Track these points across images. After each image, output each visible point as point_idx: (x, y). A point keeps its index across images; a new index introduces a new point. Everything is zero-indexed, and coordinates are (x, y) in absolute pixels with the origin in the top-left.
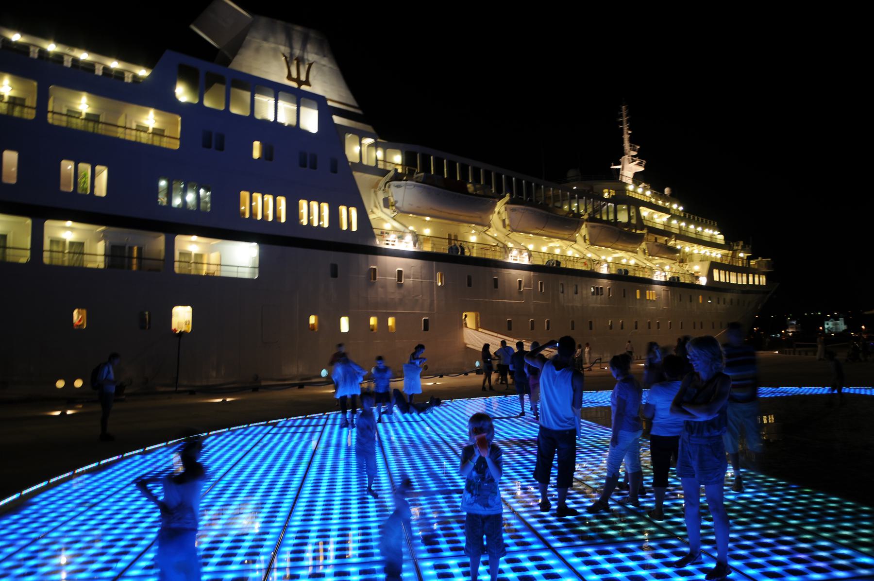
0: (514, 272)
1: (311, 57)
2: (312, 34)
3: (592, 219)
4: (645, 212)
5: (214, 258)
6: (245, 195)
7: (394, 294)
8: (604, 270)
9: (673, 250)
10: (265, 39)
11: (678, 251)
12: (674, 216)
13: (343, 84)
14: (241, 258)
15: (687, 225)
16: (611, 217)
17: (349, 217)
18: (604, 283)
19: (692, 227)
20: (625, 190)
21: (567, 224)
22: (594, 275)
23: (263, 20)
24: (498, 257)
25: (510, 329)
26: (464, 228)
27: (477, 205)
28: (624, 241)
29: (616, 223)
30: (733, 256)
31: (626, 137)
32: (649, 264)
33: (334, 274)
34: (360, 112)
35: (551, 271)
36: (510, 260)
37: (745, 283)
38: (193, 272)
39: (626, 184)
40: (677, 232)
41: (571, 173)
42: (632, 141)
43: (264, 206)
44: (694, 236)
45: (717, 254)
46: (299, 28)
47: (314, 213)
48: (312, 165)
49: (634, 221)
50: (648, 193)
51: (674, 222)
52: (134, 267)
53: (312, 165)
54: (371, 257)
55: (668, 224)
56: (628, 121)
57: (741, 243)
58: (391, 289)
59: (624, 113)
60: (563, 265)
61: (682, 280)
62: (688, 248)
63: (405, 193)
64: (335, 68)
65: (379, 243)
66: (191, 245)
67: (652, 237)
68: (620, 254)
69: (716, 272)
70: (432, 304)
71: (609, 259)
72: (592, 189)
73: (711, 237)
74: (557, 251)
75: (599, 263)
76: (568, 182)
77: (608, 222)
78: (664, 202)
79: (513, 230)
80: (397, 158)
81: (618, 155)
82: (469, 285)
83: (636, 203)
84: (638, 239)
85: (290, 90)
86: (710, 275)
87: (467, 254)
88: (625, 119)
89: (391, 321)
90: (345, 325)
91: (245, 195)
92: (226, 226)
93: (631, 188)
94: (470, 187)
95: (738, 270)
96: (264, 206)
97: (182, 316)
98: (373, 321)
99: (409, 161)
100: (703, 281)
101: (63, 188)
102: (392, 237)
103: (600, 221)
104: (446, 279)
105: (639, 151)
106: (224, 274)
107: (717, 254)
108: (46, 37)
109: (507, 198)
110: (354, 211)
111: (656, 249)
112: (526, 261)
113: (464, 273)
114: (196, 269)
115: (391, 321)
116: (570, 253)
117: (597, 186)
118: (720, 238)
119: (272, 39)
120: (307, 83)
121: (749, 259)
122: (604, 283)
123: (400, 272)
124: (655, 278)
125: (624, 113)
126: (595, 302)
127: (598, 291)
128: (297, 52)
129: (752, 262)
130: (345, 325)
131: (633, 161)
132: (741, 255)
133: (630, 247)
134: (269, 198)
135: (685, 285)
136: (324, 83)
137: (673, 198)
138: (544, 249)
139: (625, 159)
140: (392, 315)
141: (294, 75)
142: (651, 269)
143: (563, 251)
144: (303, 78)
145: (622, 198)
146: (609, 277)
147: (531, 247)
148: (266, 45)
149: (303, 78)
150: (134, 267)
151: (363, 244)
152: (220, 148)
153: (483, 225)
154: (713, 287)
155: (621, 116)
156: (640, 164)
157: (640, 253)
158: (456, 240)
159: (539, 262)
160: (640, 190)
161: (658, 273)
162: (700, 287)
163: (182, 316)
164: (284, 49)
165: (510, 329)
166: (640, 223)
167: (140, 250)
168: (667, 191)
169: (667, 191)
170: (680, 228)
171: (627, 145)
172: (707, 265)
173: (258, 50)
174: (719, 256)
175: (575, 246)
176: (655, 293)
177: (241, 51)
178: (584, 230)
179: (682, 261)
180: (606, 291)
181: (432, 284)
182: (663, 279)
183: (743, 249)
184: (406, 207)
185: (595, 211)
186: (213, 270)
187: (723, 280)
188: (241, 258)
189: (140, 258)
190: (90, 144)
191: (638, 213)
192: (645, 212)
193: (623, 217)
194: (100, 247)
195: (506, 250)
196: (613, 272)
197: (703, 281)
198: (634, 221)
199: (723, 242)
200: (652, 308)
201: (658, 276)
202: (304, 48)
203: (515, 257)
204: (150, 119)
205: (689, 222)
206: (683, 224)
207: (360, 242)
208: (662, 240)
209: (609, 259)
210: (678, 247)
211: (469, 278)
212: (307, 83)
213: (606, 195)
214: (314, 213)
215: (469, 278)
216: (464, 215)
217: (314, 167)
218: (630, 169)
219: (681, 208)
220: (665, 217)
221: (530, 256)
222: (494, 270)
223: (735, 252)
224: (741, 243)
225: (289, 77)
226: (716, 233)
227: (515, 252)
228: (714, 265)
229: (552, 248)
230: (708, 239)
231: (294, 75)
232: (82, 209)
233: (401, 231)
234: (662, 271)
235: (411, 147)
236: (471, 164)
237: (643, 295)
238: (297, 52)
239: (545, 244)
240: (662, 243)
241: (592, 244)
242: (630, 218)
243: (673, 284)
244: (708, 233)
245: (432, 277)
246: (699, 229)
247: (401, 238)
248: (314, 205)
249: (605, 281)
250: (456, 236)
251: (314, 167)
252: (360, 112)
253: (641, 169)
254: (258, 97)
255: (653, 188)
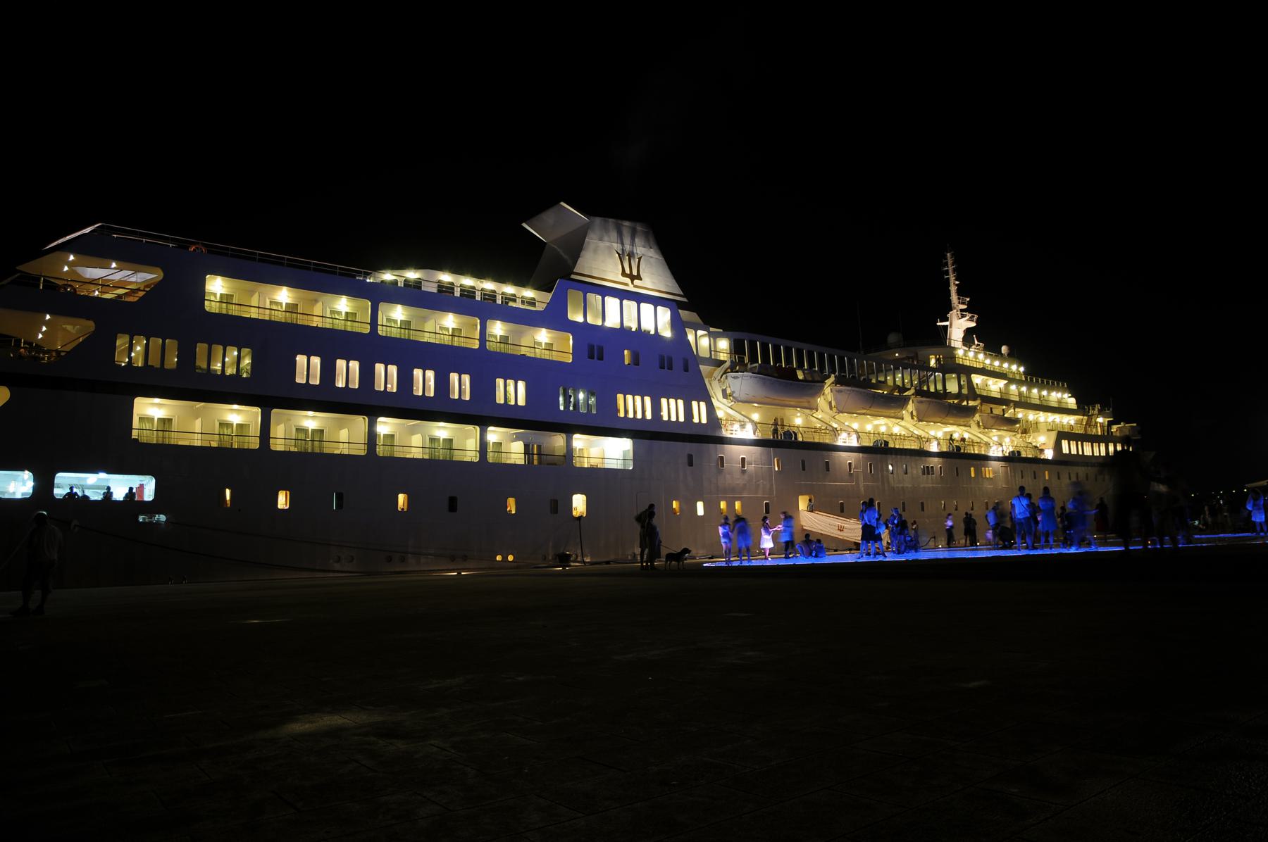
0: (844, 454)
1: (640, 250)
2: (639, 228)
3: (920, 393)
4: (977, 379)
5: (594, 452)
6: (620, 397)
7: (739, 480)
8: (934, 448)
9: (1013, 421)
10: (601, 240)
11: (1016, 421)
12: (1011, 381)
13: (668, 273)
14: (612, 452)
15: (1029, 390)
16: (940, 387)
17: (700, 413)
18: (935, 462)
19: (1035, 391)
20: (953, 357)
21: (892, 402)
22: (923, 453)
23: (598, 220)
24: (827, 440)
25: (842, 511)
26: (789, 412)
27: (808, 389)
28: (955, 416)
29: (946, 395)
30: (1088, 424)
31: (953, 289)
32: (985, 439)
33: (691, 464)
34: (685, 300)
35: (879, 451)
36: (840, 443)
37: (1103, 454)
38: (317, 450)
39: (954, 349)
40: (1017, 399)
41: (892, 338)
42: (960, 293)
43: (634, 406)
44: (1038, 402)
45: (1069, 421)
46: (627, 223)
47: (673, 410)
48: (671, 368)
49: (965, 391)
50: (981, 356)
51: (1013, 387)
52: (536, 462)
53: (671, 368)
54: (719, 446)
55: (1005, 392)
56: (954, 270)
57: (1098, 407)
58: (737, 475)
59: (950, 262)
60: (891, 445)
61: (1023, 455)
62: (1032, 416)
63: (742, 383)
64: (661, 258)
65: (726, 433)
66: (579, 441)
67: (986, 407)
68: (950, 428)
69: (1065, 443)
70: (771, 489)
71: (938, 435)
72: (916, 357)
73: (1059, 402)
74: (883, 429)
75: (928, 440)
76: (890, 348)
77: (936, 395)
78: (1002, 363)
79: (840, 412)
80: (724, 344)
81: (944, 310)
82: (804, 469)
83: (968, 371)
84: (970, 412)
85: (629, 289)
86: (1058, 447)
87: (800, 439)
88: (951, 268)
89: (738, 505)
90: (700, 509)
91: (620, 397)
92: (607, 427)
93: (960, 353)
94: (800, 376)
95: (1094, 439)
96: (634, 406)
97: (579, 503)
98: (723, 505)
99: (737, 348)
100: (1049, 454)
101: (176, 342)
102: (736, 426)
103: (927, 394)
104: (783, 464)
105: (969, 304)
106: (607, 466)
107: (1069, 421)
108: (440, 268)
109: (832, 379)
110: (703, 405)
111: (991, 421)
112: (854, 442)
113: (795, 453)
114: (320, 447)
115: (738, 505)
116: (896, 430)
117: (922, 352)
118: (1071, 402)
119: (606, 238)
120: (639, 277)
121: (1110, 424)
122: (935, 462)
123: (743, 459)
124: (991, 454)
125: (950, 262)
126: (927, 482)
127: (928, 471)
128: (628, 247)
129: (1114, 428)
130: (700, 509)
131: (963, 316)
132: (1100, 420)
133: (962, 421)
134: (638, 398)
135: (1027, 460)
136: (655, 279)
137: (1012, 356)
138: (869, 428)
139: (953, 314)
140: (739, 499)
141: (628, 271)
142: (987, 445)
143: (889, 428)
144: (635, 273)
145: (950, 366)
146: (940, 455)
147: (855, 426)
148: (601, 244)
149: (635, 273)
150: (536, 462)
151: (710, 436)
152: (601, 358)
153: (811, 409)
154: (1062, 461)
155: (946, 264)
156: (971, 319)
157: (974, 426)
158: (783, 425)
159: (867, 443)
160: (971, 354)
161: (994, 448)
162: (1046, 461)
163: (579, 503)
164: (617, 246)
165: (842, 511)
166: (973, 393)
167: (539, 447)
168: (1004, 349)
169: (1004, 349)
170: (1020, 394)
171: (954, 298)
172: (1053, 435)
173: (595, 251)
174: (1072, 422)
175: (903, 423)
176: (993, 470)
177: (583, 253)
178: (911, 406)
179: (1025, 432)
180: (937, 470)
181: (771, 469)
182: (1000, 455)
183: (1101, 413)
184: (743, 397)
185: (921, 383)
186: (594, 462)
187: (1074, 452)
188: (612, 452)
189: (539, 454)
190: (516, 366)
191: (970, 381)
192: (977, 379)
193: (952, 387)
194: (518, 447)
195: (835, 432)
196: (945, 450)
197: (1049, 454)
198: (965, 391)
199: (1075, 407)
200: (989, 486)
201: (995, 452)
202: (633, 243)
203: (844, 440)
204: (543, 336)
205: (1030, 385)
206: (1024, 389)
207: (710, 433)
208: (998, 410)
209: (938, 435)
210: (1020, 416)
211: (803, 462)
212: (639, 277)
213: (933, 363)
214: (673, 410)
215: (803, 462)
216: (793, 401)
217: (670, 368)
218: (958, 326)
219: (1022, 369)
220: (1002, 383)
221: (858, 437)
222: (825, 453)
223: (1090, 417)
224: (1098, 407)
225: (624, 274)
226: (1066, 396)
227: (844, 435)
228: (1062, 435)
229: (877, 426)
230: (1056, 405)
231: (628, 271)
232: (509, 418)
233: (739, 416)
234: (999, 444)
235: (739, 335)
236: (794, 347)
237: (978, 472)
238: (628, 247)
239: (870, 421)
240: (999, 413)
241: (920, 420)
242: (960, 387)
243: (1013, 459)
244: (1055, 397)
245: (771, 463)
246: (1044, 393)
247: (743, 426)
248: (672, 401)
249: (936, 459)
250: (782, 420)
251: (670, 368)
252: (685, 300)
253: (973, 324)
254: (589, 295)
255: (986, 349)
